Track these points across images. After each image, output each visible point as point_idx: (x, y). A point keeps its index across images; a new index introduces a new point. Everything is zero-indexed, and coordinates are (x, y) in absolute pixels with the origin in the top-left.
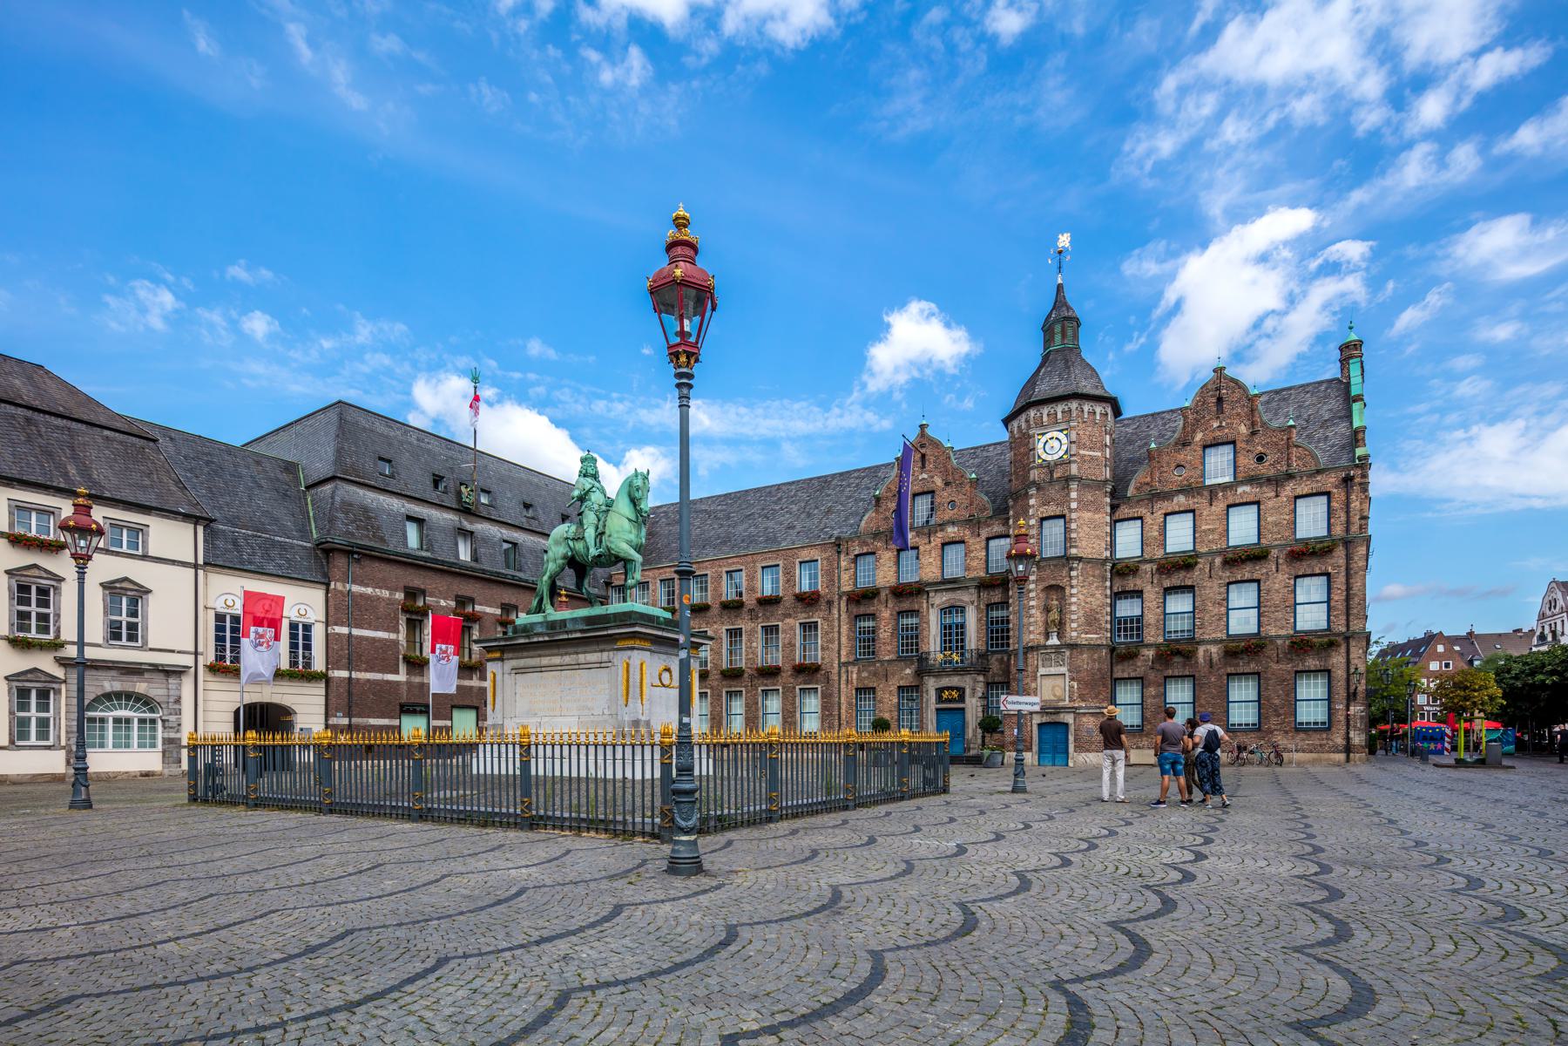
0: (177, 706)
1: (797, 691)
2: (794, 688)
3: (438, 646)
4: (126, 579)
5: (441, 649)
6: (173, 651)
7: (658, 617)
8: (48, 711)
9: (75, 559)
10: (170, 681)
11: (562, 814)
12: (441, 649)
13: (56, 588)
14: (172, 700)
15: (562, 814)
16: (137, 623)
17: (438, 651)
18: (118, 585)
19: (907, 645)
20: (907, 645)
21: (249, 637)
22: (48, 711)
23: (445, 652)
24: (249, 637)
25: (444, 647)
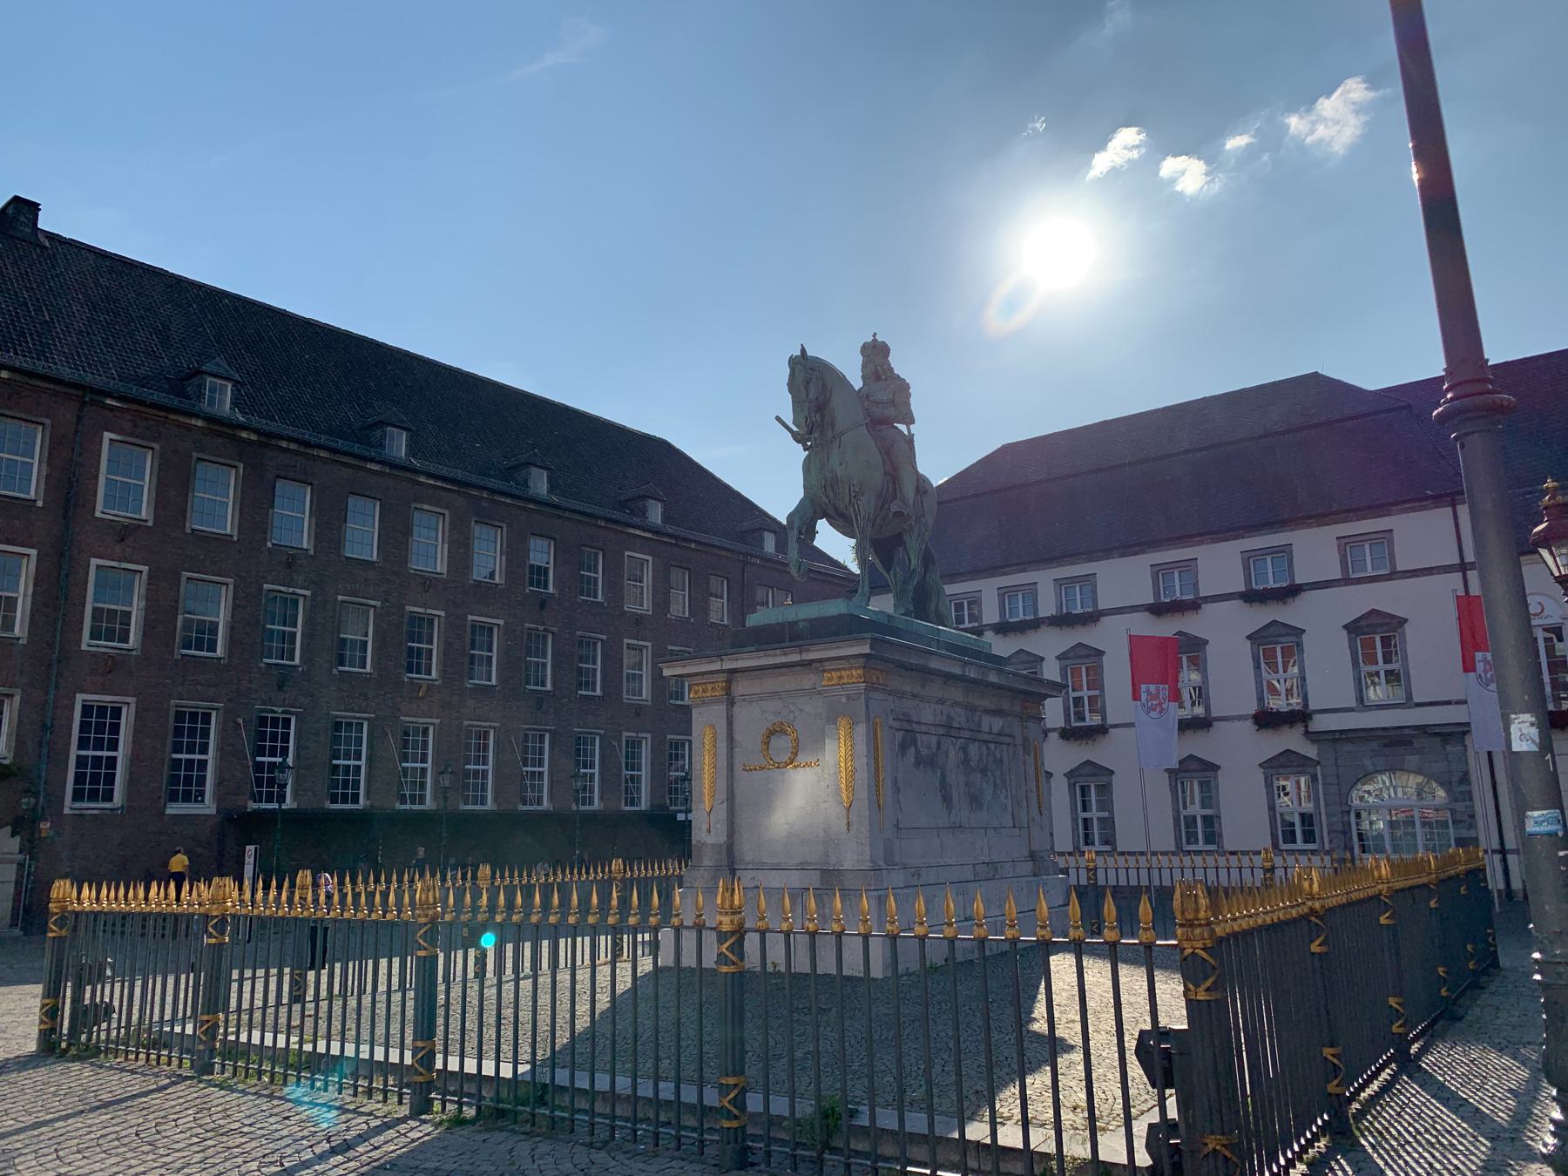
0: (1464, 788)
1: (184, 579)
2: (47, 417)
3: (1143, 687)
4: (1373, 612)
5: (1148, 691)
6: (1448, 703)
7: (793, 624)
8: (116, 750)
9: (1560, 583)
10: (1449, 748)
11: (634, 1087)
12: (1148, 691)
13: (1298, 645)
14: (1455, 779)
15: (634, 1087)
16: (207, 761)
17: (1144, 696)
18: (1363, 623)
19: (346, 782)
20: (346, 782)
21: (1474, 670)
22: (116, 750)
23: (1156, 697)
24: (1474, 670)
25: (1152, 687)
